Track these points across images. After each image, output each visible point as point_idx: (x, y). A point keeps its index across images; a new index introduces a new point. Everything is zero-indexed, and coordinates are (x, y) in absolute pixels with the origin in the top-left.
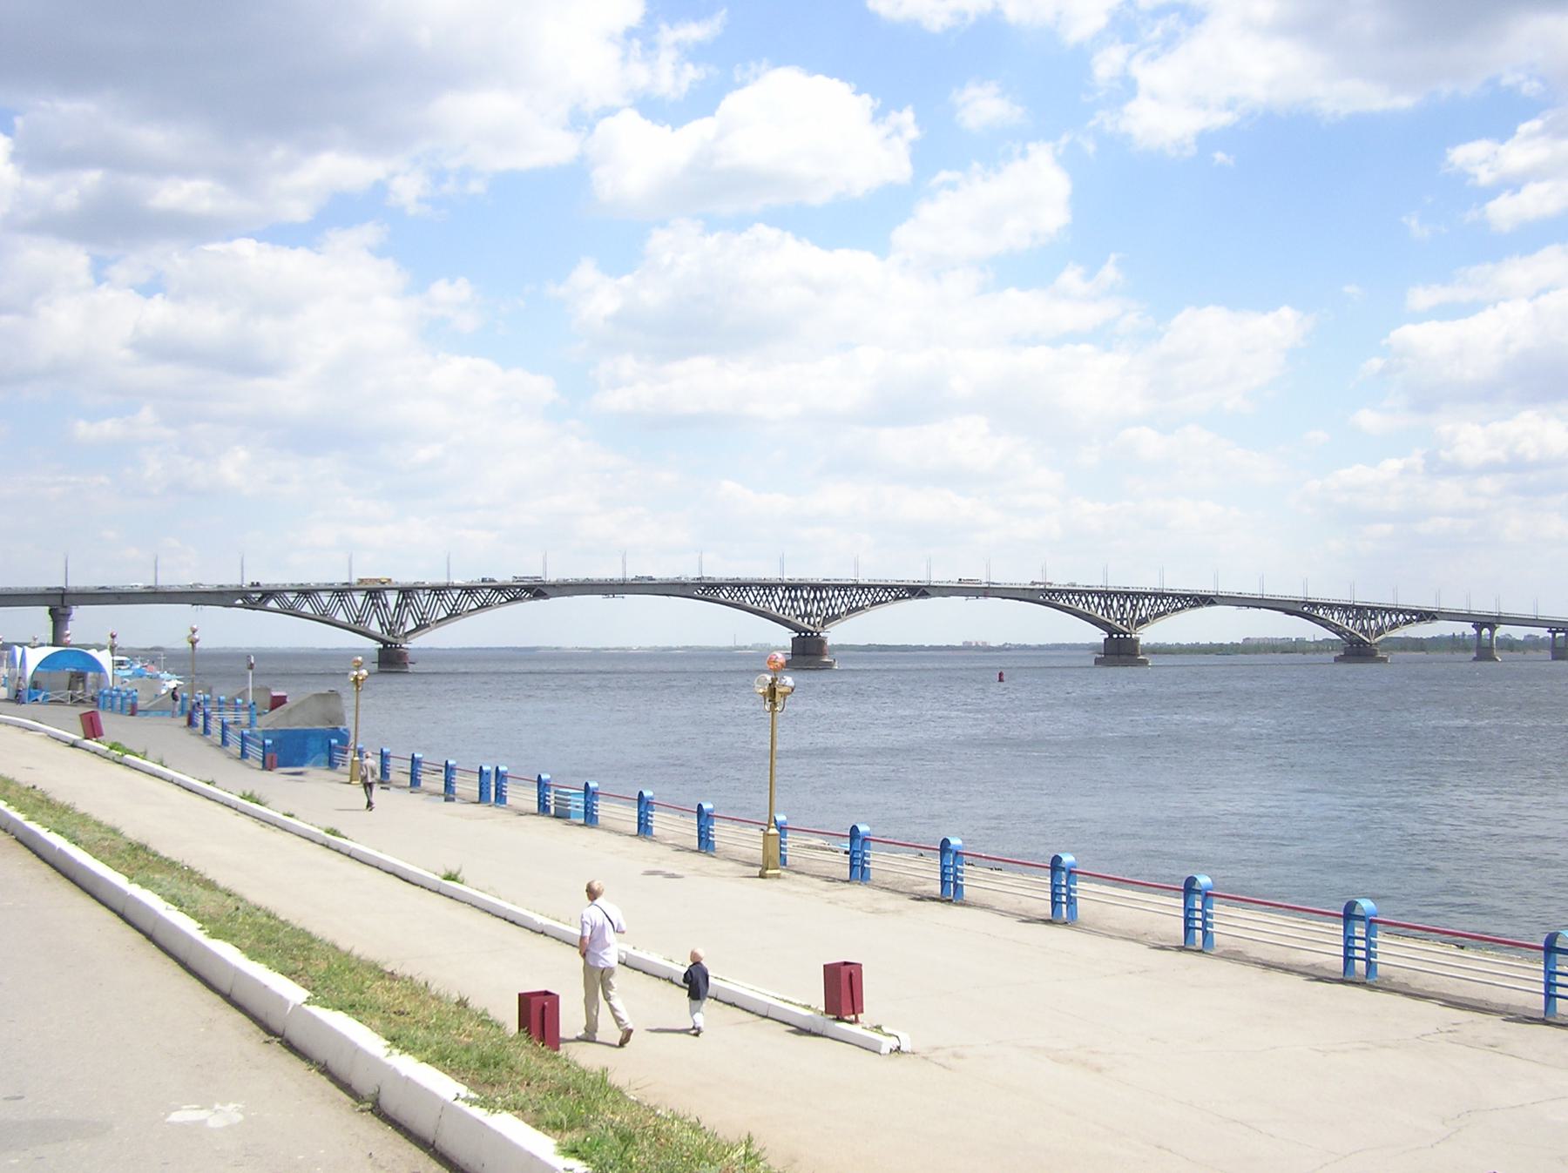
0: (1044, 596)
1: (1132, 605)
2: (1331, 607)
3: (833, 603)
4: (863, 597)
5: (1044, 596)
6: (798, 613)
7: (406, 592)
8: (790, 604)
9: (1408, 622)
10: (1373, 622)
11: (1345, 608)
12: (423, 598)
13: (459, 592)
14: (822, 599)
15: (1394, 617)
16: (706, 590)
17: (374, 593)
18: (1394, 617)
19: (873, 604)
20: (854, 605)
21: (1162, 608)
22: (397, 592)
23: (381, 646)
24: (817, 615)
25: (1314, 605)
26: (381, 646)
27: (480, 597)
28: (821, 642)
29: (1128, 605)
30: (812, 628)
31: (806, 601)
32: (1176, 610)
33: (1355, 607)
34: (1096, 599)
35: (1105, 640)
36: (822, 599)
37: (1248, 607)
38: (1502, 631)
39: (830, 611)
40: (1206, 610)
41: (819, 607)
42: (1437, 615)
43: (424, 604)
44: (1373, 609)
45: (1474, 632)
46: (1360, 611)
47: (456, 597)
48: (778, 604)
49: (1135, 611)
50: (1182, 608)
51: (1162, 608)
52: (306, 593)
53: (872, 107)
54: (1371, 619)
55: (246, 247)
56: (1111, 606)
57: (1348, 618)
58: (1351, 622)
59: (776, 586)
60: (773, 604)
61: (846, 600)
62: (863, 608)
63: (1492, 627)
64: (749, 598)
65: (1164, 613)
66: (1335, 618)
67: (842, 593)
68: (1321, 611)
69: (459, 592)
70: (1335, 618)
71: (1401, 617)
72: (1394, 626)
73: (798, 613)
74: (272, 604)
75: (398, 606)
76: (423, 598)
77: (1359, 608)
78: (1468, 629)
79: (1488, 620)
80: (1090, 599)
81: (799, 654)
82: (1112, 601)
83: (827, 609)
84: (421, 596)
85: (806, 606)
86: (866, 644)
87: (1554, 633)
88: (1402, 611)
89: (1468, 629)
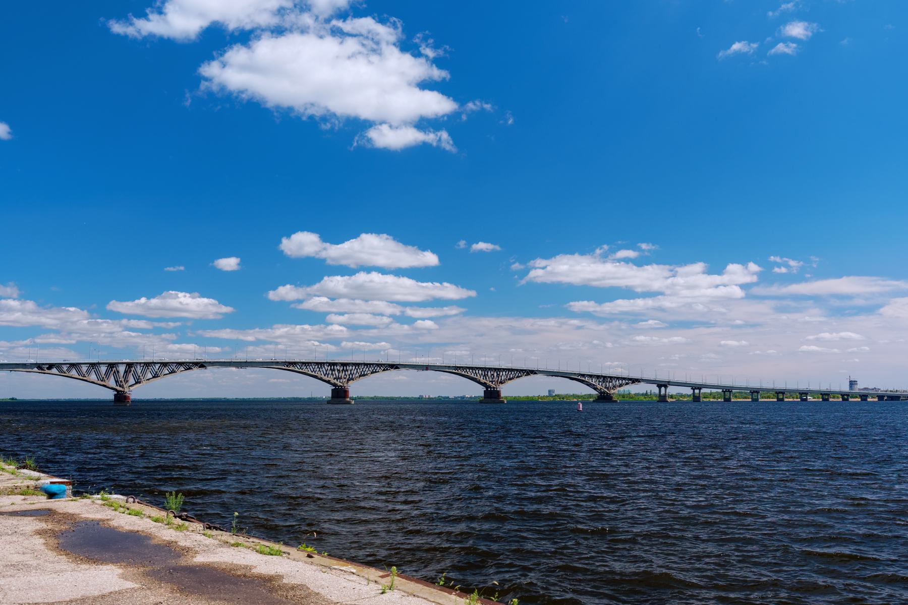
0: (457, 370)
1: (497, 374)
2: (591, 376)
3: (352, 372)
4: (367, 369)
5: (457, 370)
6: (335, 376)
7: (130, 365)
8: (330, 372)
9: (627, 384)
10: (611, 384)
11: (598, 377)
12: (139, 369)
13: (159, 365)
16: (289, 365)
19: (372, 373)
20: (363, 373)
21: (511, 376)
22: (125, 365)
23: (116, 393)
24: (344, 378)
25: (583, 375)
26: (116, 393)
28: (498, 393)
29: (495, 374)
30: (341, 384)
31: (338, 370)
32: (518, 377)
33: (602, 376)
34: (480, 372)
35: (115, 395)
36: (347, 370)
37: (552, 376)
38: (704, 390)
39: (351, 376)
40: (532, 376)
41: (345, 374)
42: (399, 366)
44: (611, 378)
45: (658, 389)
46: (604, 378)
47: (157, 367)
48: (325, 372)
49: (498, 377)
50: (521, 376)
51: (511, 376)
53: (366, 282)
54: (610, 382)
55: (419, 322)
56: (487, 375)
57: (599, 382)
58: (600, 383)
59: (362, 364)
60: (322, 373)
61: (359, 370)
62: (367, 375)
63: (700, 389)
65: (513, 378)
66: (593, 381)
68: (587, 378)
69: (159, 365)
70: (593, 381)
72: (621, 386)
73: (335, 376)
74: (54, 371)
75: (126, 372)
77: (605, 377)
78: (654, 389)
79: (663, 383)
80: (477, 371)
81: (488, 398)
82: (488, 372)
83: (349, 375)
85: (339, 373)
86: (417, 396)
87: (694, 390)
88: (624, 379)
89: (654, 389)
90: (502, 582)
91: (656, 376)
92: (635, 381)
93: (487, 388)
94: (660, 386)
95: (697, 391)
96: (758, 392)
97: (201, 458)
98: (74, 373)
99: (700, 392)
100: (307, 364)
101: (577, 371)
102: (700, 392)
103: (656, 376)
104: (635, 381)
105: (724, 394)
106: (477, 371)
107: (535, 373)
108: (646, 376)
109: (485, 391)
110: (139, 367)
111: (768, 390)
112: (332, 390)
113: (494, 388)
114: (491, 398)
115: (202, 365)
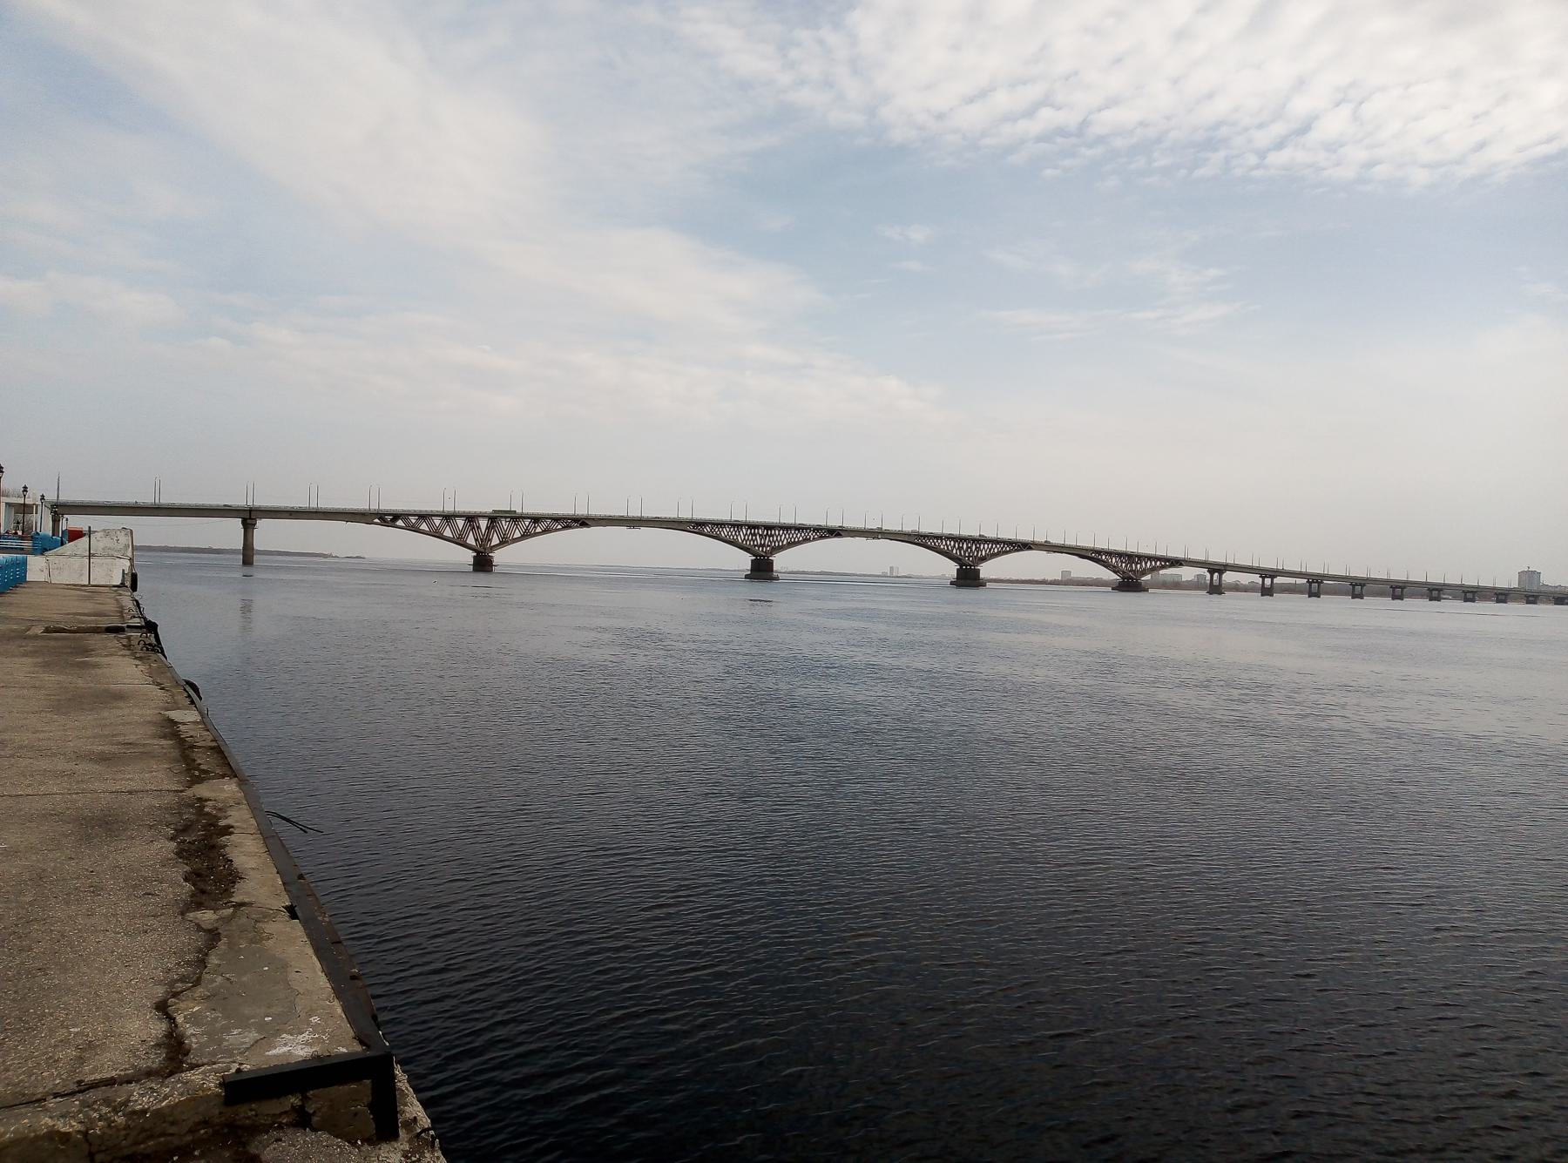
7: (493, 519)
14: (772, 535)
15: (1153, 563)
17: (471, 519)
18: (1153, 563)
23: (475, 554)
24: (768, 546)
26: (475, 554)
27: (544, 525)
36: (772, 535)
37: (1055, 552)
38: (1278, 580)
39: (777, 544)
41: (769, 540)
43: (505, 528)
45: (1261, 579)
46: (1130, 557)
47: (527, 523)
51: (996, 550)
52: (423, 517)
64: (724, 532)
67: (781, 532)
71: (1158, 563)
72: (1153, 569)
75: (487, 528)
76: (504, 524)
80: (948, 543)
82: (963, 544)
84: (503, 522)
85: (761, 540)
87: (1263, 579)
89: (229, 533)
90: (185, 1017)
91: (1207, 552)
92: (1176, 563)
93: (961, 567)
94: (1212, 572)
95: (1268, 581)
96: (1402, 588)
97: (1172, 870)
98: (424, 527)
99: (1402, 592)
100: (721, 524)
101: (1090, 545)
102: (1272, 582)
103: (1207, 552)
104: (1176, 563)
105: (1310, 586)
106: (948, 543)
107: (1030, 548)
108: (1193, 556)
109: (958, 569)
110: (503, 522)
111: (1375, 581)
112: (752, 561)
113: (971, 566)
114: (759, 571)
115: (583, 522)
